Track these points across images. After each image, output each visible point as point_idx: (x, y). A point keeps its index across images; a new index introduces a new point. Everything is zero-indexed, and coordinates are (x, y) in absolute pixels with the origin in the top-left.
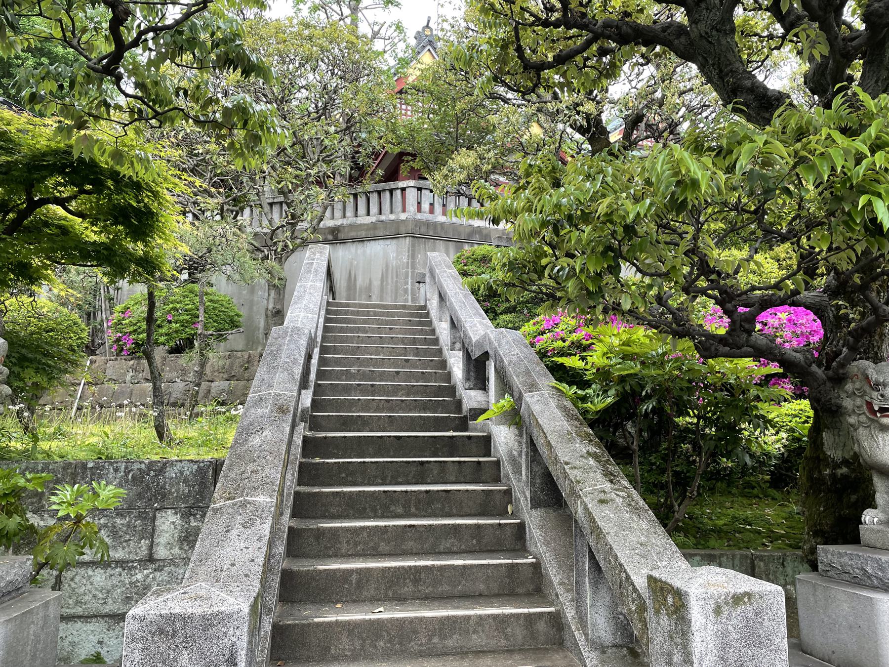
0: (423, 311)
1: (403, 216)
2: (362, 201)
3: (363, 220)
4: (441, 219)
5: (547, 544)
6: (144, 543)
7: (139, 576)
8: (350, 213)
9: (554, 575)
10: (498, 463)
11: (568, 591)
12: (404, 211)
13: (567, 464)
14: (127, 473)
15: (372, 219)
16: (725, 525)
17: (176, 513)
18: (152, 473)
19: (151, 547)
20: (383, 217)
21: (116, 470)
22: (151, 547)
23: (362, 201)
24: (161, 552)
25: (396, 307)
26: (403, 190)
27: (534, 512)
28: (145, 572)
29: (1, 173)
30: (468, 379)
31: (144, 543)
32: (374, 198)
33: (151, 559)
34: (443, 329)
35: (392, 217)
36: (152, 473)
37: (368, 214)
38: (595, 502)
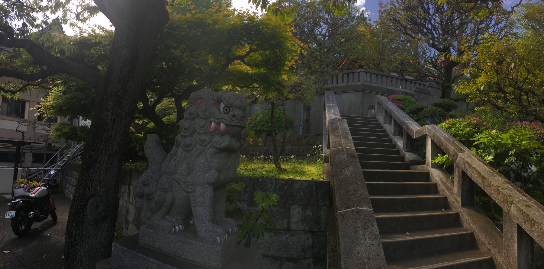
0: (374, 121)
1: (358, 83)
2: (335, 78)
3: (340, 85)
4: (375, 85)
5: (475, 224)
6: (285, 221)
7: (284, 238)
8: (335, 82)
9: (481, 237)
10: (436, 185)
11: (494, 247)
12: (359, 81)
13: (499, 187)
14: (276, 185)
15: (344, 84)
16: (34, 187)
17: (299, 207)
18: (288, 186)
19: (289, 223)
20: (350, 84)
21: (272, 183)
22: (289, 223)
23: (335, 78)
24: (293, 226)
25: (362, 117)
26: (359, 73)
27: (463, 208)
28: (287, 236)
29: (9, 153)
30: (407, 148)
31: (285, 221)
32: (345, 76)
33: (289, 229)
34: (389, 129)
35: (354, 84)
36: (288, 186)
37: (343, 82)
38: (524, 206)
